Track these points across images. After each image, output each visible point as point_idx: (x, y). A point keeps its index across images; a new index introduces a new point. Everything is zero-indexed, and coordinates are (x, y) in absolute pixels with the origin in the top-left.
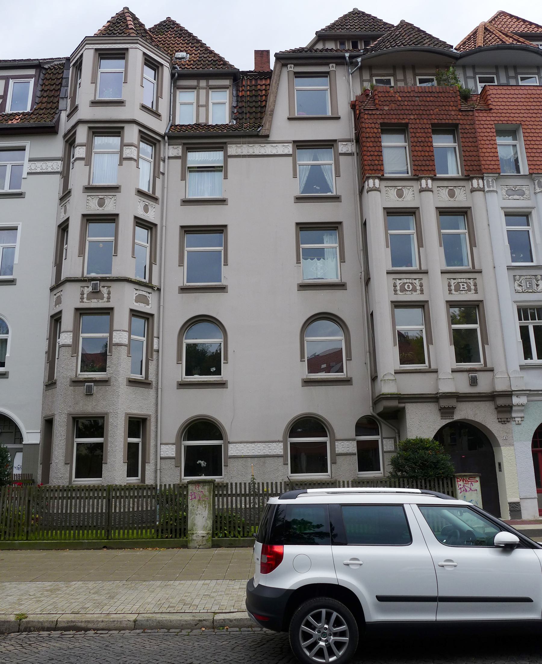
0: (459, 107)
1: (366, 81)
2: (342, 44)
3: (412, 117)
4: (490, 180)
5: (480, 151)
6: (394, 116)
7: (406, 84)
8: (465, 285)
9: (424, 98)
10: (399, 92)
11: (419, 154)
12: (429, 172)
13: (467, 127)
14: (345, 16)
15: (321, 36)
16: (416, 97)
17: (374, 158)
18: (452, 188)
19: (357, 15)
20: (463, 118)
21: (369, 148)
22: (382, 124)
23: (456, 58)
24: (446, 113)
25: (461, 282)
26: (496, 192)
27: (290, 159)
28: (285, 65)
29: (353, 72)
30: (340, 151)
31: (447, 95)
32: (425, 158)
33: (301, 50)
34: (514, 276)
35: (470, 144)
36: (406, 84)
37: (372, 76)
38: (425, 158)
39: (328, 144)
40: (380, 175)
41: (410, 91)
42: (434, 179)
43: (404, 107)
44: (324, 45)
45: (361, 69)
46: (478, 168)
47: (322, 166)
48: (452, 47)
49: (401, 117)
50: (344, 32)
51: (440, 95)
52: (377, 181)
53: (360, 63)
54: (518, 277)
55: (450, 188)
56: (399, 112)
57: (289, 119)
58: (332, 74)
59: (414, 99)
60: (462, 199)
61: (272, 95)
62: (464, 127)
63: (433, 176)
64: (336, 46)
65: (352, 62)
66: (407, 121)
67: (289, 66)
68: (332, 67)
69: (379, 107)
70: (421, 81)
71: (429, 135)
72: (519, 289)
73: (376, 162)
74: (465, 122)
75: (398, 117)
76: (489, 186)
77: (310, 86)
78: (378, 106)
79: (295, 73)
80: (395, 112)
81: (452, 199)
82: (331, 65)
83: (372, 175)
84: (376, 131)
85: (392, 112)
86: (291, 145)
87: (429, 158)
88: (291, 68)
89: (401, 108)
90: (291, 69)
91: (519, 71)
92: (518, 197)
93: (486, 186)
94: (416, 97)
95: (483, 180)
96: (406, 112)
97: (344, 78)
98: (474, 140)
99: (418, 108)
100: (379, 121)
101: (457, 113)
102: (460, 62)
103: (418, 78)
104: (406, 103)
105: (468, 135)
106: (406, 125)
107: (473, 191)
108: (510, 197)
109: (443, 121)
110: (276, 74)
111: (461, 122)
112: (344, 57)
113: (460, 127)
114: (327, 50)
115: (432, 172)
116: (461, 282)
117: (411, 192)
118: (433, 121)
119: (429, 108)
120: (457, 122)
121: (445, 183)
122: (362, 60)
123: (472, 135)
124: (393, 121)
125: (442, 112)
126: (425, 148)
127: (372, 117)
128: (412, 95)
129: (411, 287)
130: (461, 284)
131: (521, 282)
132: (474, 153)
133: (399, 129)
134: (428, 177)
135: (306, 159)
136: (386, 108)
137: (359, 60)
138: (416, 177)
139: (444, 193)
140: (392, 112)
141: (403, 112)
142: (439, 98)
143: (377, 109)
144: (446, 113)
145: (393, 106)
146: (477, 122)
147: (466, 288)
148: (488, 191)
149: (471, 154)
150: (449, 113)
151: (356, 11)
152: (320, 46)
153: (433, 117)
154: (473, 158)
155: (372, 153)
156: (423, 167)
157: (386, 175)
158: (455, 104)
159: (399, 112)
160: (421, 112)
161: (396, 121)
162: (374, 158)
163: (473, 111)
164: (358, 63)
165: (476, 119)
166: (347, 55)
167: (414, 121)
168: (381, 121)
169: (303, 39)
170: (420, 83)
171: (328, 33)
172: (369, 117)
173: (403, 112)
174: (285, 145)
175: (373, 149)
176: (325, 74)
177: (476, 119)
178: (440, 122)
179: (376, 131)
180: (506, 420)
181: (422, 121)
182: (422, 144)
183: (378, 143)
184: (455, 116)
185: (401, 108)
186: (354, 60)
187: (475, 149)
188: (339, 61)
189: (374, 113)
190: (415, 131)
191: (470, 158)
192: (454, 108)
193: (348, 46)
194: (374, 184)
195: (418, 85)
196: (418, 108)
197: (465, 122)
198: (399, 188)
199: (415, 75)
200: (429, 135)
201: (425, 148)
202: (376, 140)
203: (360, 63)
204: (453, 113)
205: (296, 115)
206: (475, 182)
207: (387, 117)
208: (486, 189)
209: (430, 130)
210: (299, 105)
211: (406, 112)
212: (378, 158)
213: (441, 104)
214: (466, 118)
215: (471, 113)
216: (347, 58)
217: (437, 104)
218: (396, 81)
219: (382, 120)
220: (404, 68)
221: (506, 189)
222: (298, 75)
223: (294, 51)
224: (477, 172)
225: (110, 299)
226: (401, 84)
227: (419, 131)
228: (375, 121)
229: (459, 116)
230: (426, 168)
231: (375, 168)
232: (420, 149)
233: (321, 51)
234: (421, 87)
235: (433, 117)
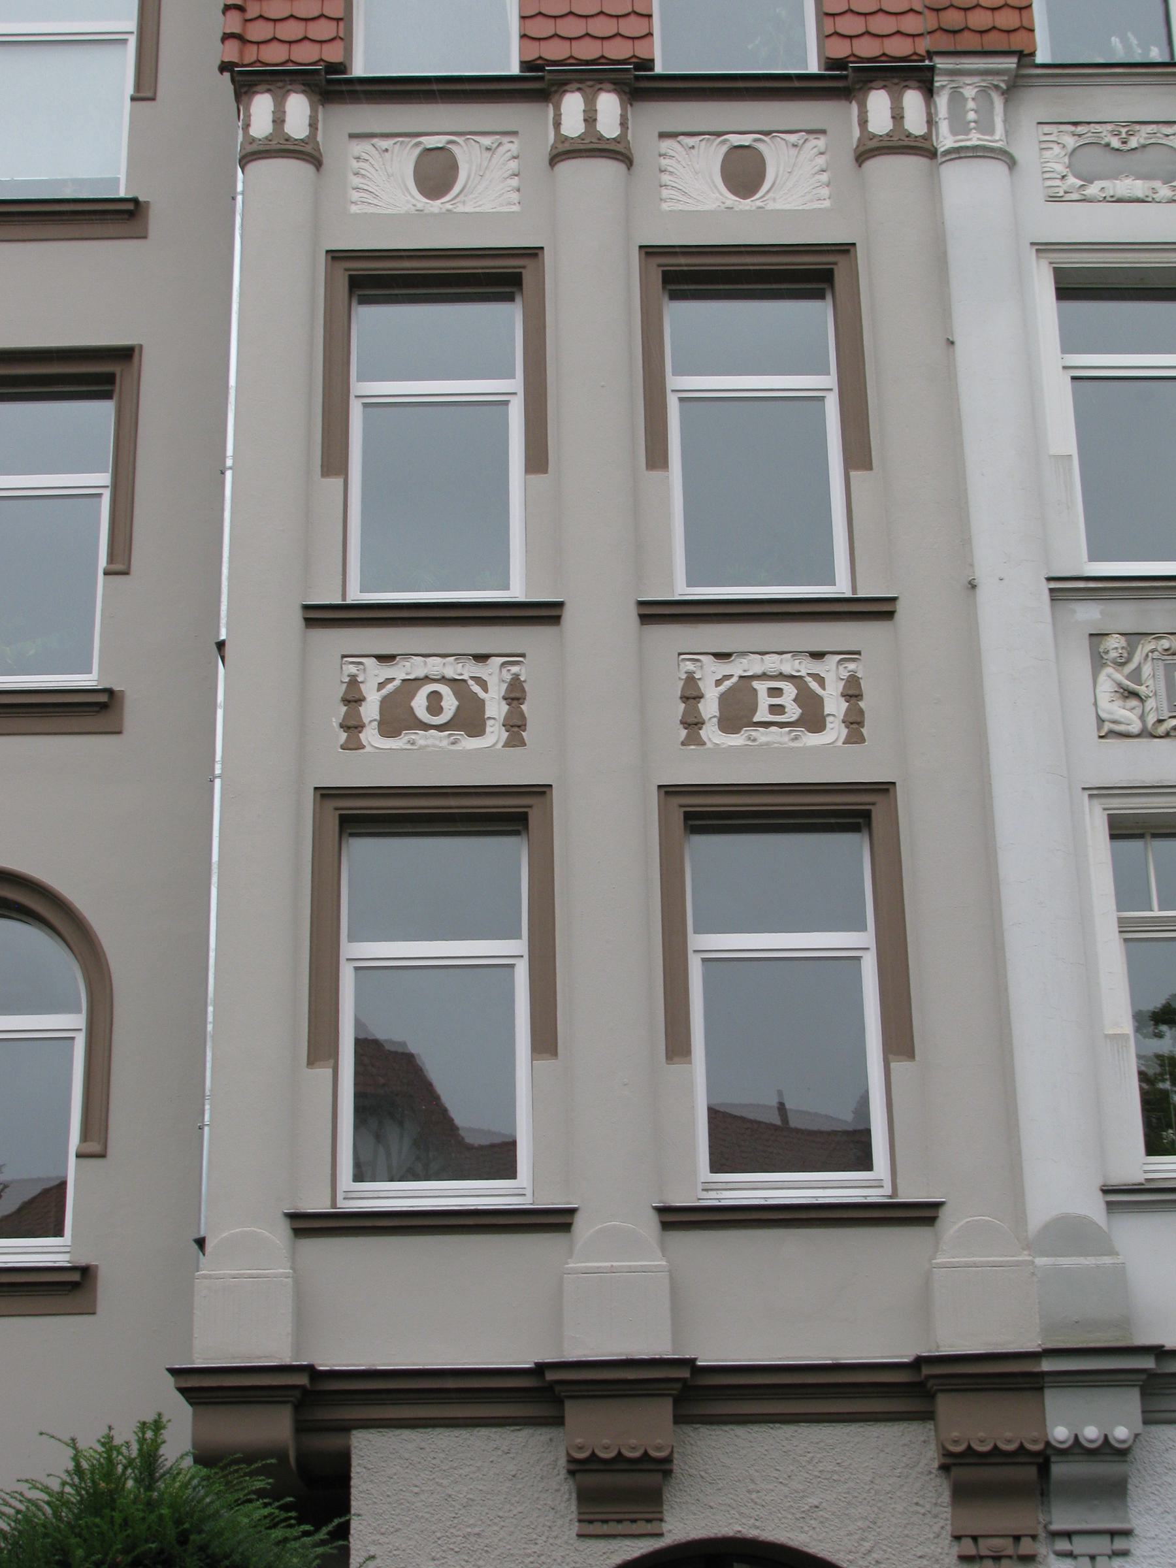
4: (969, 92)
8: (790, 690)
25: (764, 676)
26: (1011, 162)
34: (1097, 637)
54: (1115, 644)
72: (1126, 715)
76: (959, 125)
92: (1139, 188)
93: (944, 127)
95: (929, 92)
108: (1093, 190)
116: (764, 676)
129: (450, 703)
130: (761, 687)
131: (1136, 675)
147: (793, 712)
148: (958, 153)
180: (1007, 1546)
208: (946, 140)
221: (1071, 142)
225: (860, 724)
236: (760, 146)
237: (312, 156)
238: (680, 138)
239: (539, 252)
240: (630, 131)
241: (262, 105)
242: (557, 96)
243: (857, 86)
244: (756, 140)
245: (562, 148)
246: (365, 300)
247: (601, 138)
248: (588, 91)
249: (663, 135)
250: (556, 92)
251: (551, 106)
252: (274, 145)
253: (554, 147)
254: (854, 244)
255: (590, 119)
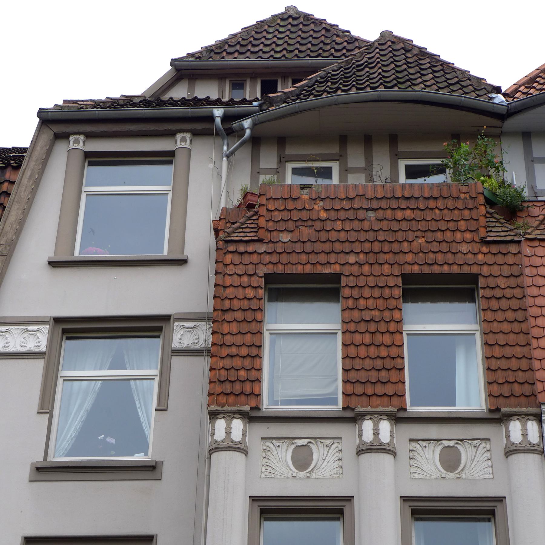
0: (482, 233)
1: (356, 170)
2: (238, 85)
3: (352, 259)
5: (534, 343)
6: (304, 258)
7: (370, 178)
9: (389, 212)
10: (322, 199)
11: (363, 352)
12: (385, 399)
13: (502, 282)
14: (261, 23)
15: (185, 70)
16: (367, 210)
17: (238, 362)
18: (451, 443)
19: (294, 23)
20: (490, 259)
21: (229, 337)
22: (407, 278)
23: (502, 115)
24: (445, 247)
27: (39, 365)
28: (65, 136)
29: (232, 153)
30: (176, 344)
31: (450, 204)
32: (378, 363)
33: (128, 101)
35: (506, 327)
36: (370, 178)
37: (282, 160)
38: (378, 363)
39: (150, 326)
40: (247, 408)
41: (352, 195)
42: (399, 418)
43: (333, 236)
44: (191, 88)
45: (256, 142)
46: (527, 389)
47: (132, 382)
48: (498, 90)
49: (323, 258)
50: (242, 61)
51: (432, 204)
52: (385, 426)
53: (248, 132)
55: (446, 443)
56: (318, 247)
57: (53, 264)
58: (179, 158)
59: (361, 214)
60: (478, 472)
61: (15, 207)
62: (491, 282)
63: (394, 410)
64: (222, 90)
65: (230, 128)
66: (336, 268)
67: (72, 138)
68: (182, 142)
69: (268, 236)
70: (412, 172)
71: (393, 303)
73: (243, 373)
74: (495, 270)
75: (313, 258)
77: (124, 184)
78: (262, 234)
79: (87, 155)
80: (308, 247)
81: (451, 475)
82: (179, 136)
83: (227, 408)
84: (250, 293)
85: (299, 248)
86: (46, 329)
87: (388, 364)
88: (78, 143)
89: (324, 236)
90: (76, 146)
91: (402, 148)
94: (367, 210)
96: (338, 247)
97: (211, 166)
98: (520, 315)
99: (371, 236)
100: (262, 270)
101: (476, 247)
102: (511, 123)
103: (402, 164)
104: (339, 225)
105: (504, 304)
106: (336, 278)
107: (511, 451)
109: (436, 269)
110: (34, 158)
111: (485, 270)
112: (211, 119)
113: (481, 282)
114: (196, 102)
115: (395, 400)
117: (332, 454)
118: (408, 270)
119: (400, 236)
120: (475, 270)
121: (433, 431)
122: (254, 125)
123: (514, 304)
124: (299, 269)
125: (435, 247)
126: (379, 338)
127: (246, 259)
128: (356, 206)
132: (518, 349)
133: (319, 288)
134: (381, 414)
135: (89, 366)
136: (285, 237)
137: (247, 123)
138: (497, 416)
139: (429, 458)
140: (299, 248)
141: (328, 247)
142: (428, 212)
143: (261, 241)
144: (445, 247)
145: (304, 232)
146: (527, 271)
149: (508, 351)
150: (454, 248)
151: (292, 12)
152: (180, 92)
153: (410, 258)
154: (514, 364)
155: (233, 350)
156: (373, 385)
157: (414, 410)
158: (473, 225)
159: (318, 247)
160: (377, 247)
161: (308, 269)
162: (238, 362)
163: (519, 242)
164: (242, 130)
165: (526, 261)
166: (218, 112)
167: (355, 269)
168: (269, 269)
169: (136, 75)
170: (408, 177)
171: (205, 62)
172: (237, 259)
173: (328, 247)
174: (30, 328)
175: (239, 340)
176: (166, 158)
177: (526, 261)
178: (426, 270)
179: (250, 293)
181: (377, 270)
182: (372, 327)
183: (254, 324)
184: (470, 256)
185: (324, 236)
186: (235, 125)
187: (522, 339)
188: (198, 126)
189: (251, 249)
190: (356, 293)
191: (504, 364)
192: (468, 236)
193: (252, 91)
194: (525, 435)
195: (402, 179)
196: (371, 236)
197: (495, 270)
198: (300, 442)
199: (396, 156)
200: (393, 303)
201: (379, 338)
202: (250, 316)
203: (248, 132)
204: (464, 248)
205: (77, 254)
206: (515, 427)
207: (285, 258)
209: (398, 292)
210: (88, 231)
211: (338, 247)
212: (247, 363)
213: (433, 226)
214: (500, 259)
215: (513, 249)
216: (218, 120)
217: (423, 226)
218: (345, 171)
219: (270, 266)
220: (368, 141)
222: (93, 159)
223: (113, 103)
224: (523, 400)
226: (356, 180)
227: (367, 292)
228: (251, 269)
229: (480, 257)
230: (379, 389)
231: (238, 388)
232: (367, 338)
233: (184, 102)
234: (412, 185)
235: (410, 258)
236: (458, 446)
237: (244, 450)
238: (420, 442)
239: (352, 499)
240: (247, 437)
241: (221, 424)
242: (360, 421)
243: (505, 418)
244: (309, 443)
245: (214, 446)
246: (266, 519)
247: (381, 443)
248: (228, 418)
249: (411, 440)
250: (359, 419)
251: (503, 426)
252: (225, 444)
253: (358, 447)
254: (505, 497)
255: (376, 434)
